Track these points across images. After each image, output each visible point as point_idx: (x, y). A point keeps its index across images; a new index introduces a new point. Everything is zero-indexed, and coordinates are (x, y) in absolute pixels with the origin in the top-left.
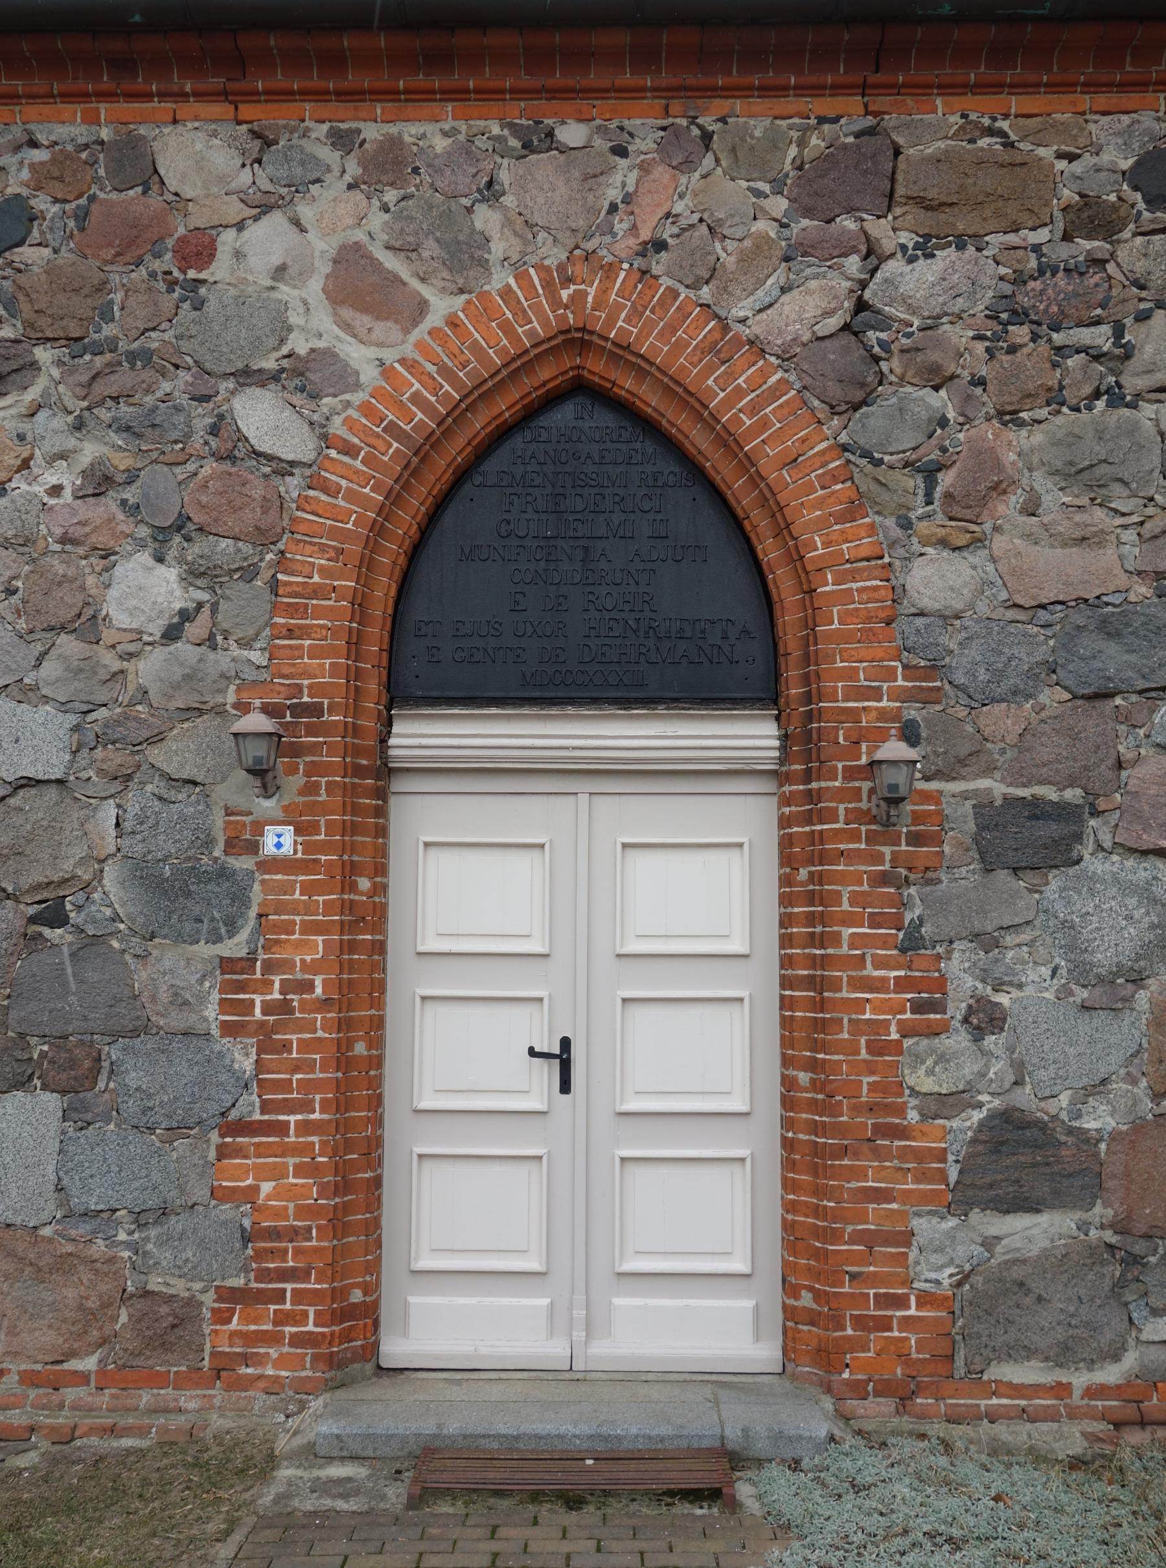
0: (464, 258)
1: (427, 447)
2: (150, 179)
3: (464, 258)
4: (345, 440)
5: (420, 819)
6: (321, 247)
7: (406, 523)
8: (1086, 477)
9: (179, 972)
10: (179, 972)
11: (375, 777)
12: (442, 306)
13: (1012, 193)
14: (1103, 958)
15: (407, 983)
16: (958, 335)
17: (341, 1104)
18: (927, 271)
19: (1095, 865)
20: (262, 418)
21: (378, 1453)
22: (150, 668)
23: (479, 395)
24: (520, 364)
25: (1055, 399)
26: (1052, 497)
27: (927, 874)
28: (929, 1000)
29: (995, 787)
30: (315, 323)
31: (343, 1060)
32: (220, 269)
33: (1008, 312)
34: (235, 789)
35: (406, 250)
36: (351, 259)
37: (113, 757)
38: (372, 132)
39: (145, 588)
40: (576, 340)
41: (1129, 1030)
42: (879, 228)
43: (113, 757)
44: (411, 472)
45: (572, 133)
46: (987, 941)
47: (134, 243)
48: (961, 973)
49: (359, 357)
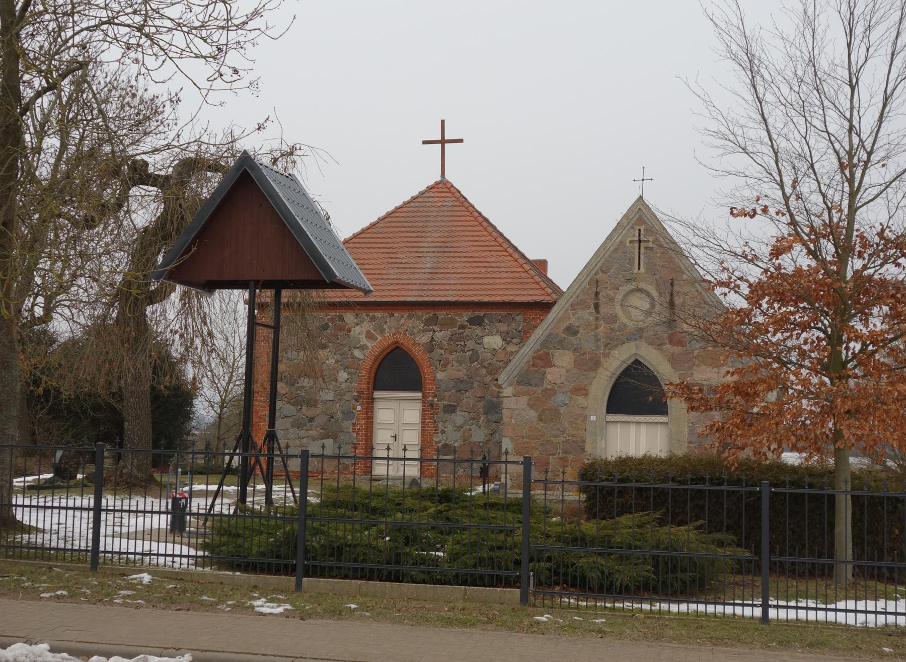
0: (382, 331)
1: (377, 357)
2: (343, 320)
3: (382, 331)
5: (378, 405)
6: (364, 330)
7: (376, 366)
8: (460, 362)
9: (347, 424)
10: (347, 424)
11: (371, 400)
12: (380, 338)
13: (452, 323)
14: (458, 424)
15: (376, 427)
16: (444, 343)
17: (366, 441)
18: (441, 334)
19: (458, 413)
20: (357, 353)
21: (332, 314)
22: (343, 386)
23: (384, 350)
24: (389, 346)
25: (456, 351)
26: (455, 364)
27: (437, 413)
28: (436, 429)
29: (446, 402)
30: (364, 341)
31: (366, 436)
32: (352, 333)
33: (451, 339)
34: (353, 402)
35: (375, 330)
36: (368, 332)
37: (339, 397)
38: (371, 314)
39: (343, 375)
41: (460, 434)
42: (435, 328)
43: (339, 397)
44: (375, 361)
45: (396, 315)
46: (444, 422)
47: (341, 329)
48: (440, 426)
49: (369, 345)
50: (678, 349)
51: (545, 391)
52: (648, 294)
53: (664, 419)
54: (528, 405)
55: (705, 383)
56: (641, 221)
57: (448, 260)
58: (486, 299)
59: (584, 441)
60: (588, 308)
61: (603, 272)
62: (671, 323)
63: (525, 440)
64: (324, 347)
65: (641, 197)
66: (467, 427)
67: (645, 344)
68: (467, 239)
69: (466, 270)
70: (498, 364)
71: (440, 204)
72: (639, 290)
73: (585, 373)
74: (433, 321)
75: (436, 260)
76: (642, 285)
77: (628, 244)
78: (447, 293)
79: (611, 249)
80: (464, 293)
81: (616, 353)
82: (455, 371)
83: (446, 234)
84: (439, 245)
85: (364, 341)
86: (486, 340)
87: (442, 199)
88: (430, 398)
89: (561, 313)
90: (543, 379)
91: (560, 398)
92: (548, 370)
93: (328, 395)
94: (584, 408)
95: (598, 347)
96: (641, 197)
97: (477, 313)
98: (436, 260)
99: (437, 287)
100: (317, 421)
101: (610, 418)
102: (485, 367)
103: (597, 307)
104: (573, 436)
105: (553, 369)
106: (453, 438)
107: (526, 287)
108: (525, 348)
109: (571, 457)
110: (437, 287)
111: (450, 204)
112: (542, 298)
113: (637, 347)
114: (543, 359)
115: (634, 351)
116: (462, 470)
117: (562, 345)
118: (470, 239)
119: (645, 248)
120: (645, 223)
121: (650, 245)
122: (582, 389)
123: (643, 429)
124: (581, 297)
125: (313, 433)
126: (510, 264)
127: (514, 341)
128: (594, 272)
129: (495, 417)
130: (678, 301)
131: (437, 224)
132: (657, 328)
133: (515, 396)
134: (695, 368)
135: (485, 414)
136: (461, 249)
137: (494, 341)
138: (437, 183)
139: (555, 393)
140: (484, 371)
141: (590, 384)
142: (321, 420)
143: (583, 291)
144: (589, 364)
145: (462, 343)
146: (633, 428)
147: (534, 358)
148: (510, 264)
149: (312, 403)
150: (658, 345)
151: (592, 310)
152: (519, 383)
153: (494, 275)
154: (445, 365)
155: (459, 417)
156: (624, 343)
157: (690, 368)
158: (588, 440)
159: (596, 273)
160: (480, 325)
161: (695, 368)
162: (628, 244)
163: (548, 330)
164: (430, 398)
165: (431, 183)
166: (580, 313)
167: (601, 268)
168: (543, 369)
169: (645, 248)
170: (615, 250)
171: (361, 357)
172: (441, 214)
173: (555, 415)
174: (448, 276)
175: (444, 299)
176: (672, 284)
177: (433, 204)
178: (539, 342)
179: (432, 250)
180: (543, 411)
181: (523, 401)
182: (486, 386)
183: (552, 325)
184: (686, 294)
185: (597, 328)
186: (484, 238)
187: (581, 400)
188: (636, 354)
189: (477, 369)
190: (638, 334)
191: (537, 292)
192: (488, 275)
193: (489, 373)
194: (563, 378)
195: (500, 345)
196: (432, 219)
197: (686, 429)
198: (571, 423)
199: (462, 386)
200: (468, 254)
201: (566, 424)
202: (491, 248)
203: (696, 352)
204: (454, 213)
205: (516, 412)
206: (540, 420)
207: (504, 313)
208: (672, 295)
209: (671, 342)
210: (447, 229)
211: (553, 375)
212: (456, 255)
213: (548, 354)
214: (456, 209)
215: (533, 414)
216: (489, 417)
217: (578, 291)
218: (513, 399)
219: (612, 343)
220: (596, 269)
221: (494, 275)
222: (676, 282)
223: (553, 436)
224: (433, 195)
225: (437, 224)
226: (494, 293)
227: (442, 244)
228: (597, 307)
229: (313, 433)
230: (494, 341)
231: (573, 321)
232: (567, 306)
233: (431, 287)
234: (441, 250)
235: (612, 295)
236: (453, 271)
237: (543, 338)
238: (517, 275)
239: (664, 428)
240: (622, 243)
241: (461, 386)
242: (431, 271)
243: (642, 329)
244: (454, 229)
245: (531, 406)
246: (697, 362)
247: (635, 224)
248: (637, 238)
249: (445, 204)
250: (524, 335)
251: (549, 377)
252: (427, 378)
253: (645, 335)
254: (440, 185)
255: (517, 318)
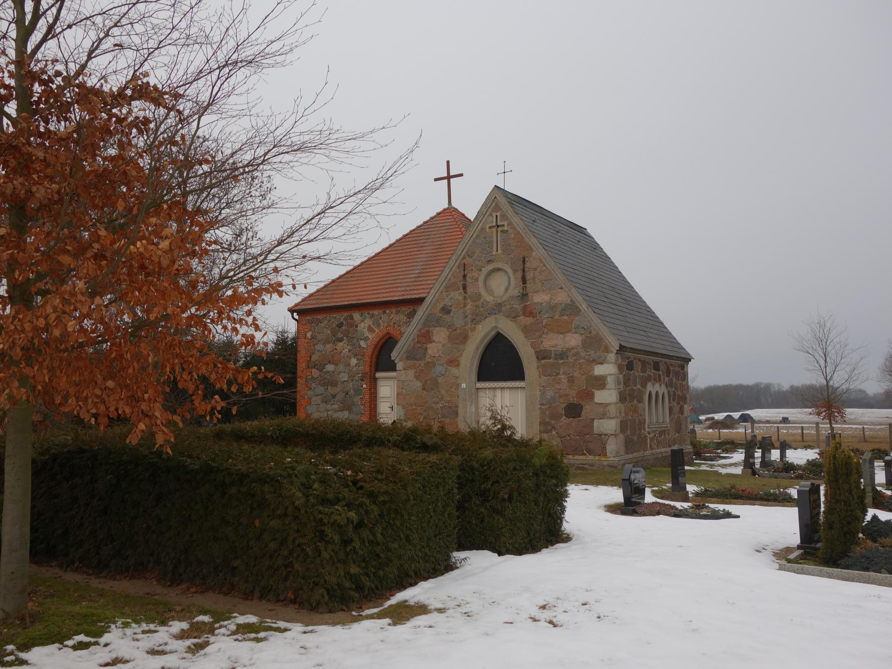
0: (378, 325)
1: (376, 346)
2: (352, 319)
3: (378, 325)
4: (316, 625)
5: (380, 383)
6: (367, 325)
7: (376, 353)
9: (357, 399)
11: (376, 379)
15: (379, 400)
20: (362, 343)
21: (345, 314)
23: (380, 340)
24: (384, 336)
30: (367, 334)
31: (370, 407)
36: (369, 326)
39: (354, 361)
40: (388, 333)
47: (351, 325)
49: (370, 336)
50: (529, 320)
51: (428, 363)
53: (394, 374)
59: (457, 407)
62: (524, 296)
64: (341, 340)
67: (503, 317)
77: (487, 230)
85: (367, 334)
91: (439, 369)
92: (429, 346)
93: (344, 377)
94: (457, 378)
95: (466, 323)
100: (339, 397)
101: (480, 385)
104: (449, 402)
113: (497, 320)
114: (425, 337)
117: (438, 323)
119: (502, 231)
121: (505, 228)
123: (507, 393)
124: (453, 280)
125: (335, 407)
139: (434, 365)
141: (461, 356)
142: (340, 396)
146: (498, 393)
147: (418, 336)
149: (334, 384)
150: (514, 317)
151: (461, 291)
152: (408, 358)
156: (486, 317)
157: (540, 336)
158: (460, 405)
159: (464, 258)
162: (487, 230)
165: (440, 209)
167: (467, 252)
169: (502, 231)
171: (365, 346)
180: (426, 382)
185: (465, 306)
187: (454, 370)
190: (498, 308)
198: (447, 391)
203: (545, 321)
208: (524, 271)
209: (524, 314)
211: (433, 349)
213: (428, 332)
215: (419, 384)
219: (477, 318)
222: (527, 259)
229: (335, 407)
231: (447, 302)
240: (483, 229)
243: (500, 304)
247: (493, 211)
250: (411, 315)
251: (430, 352)
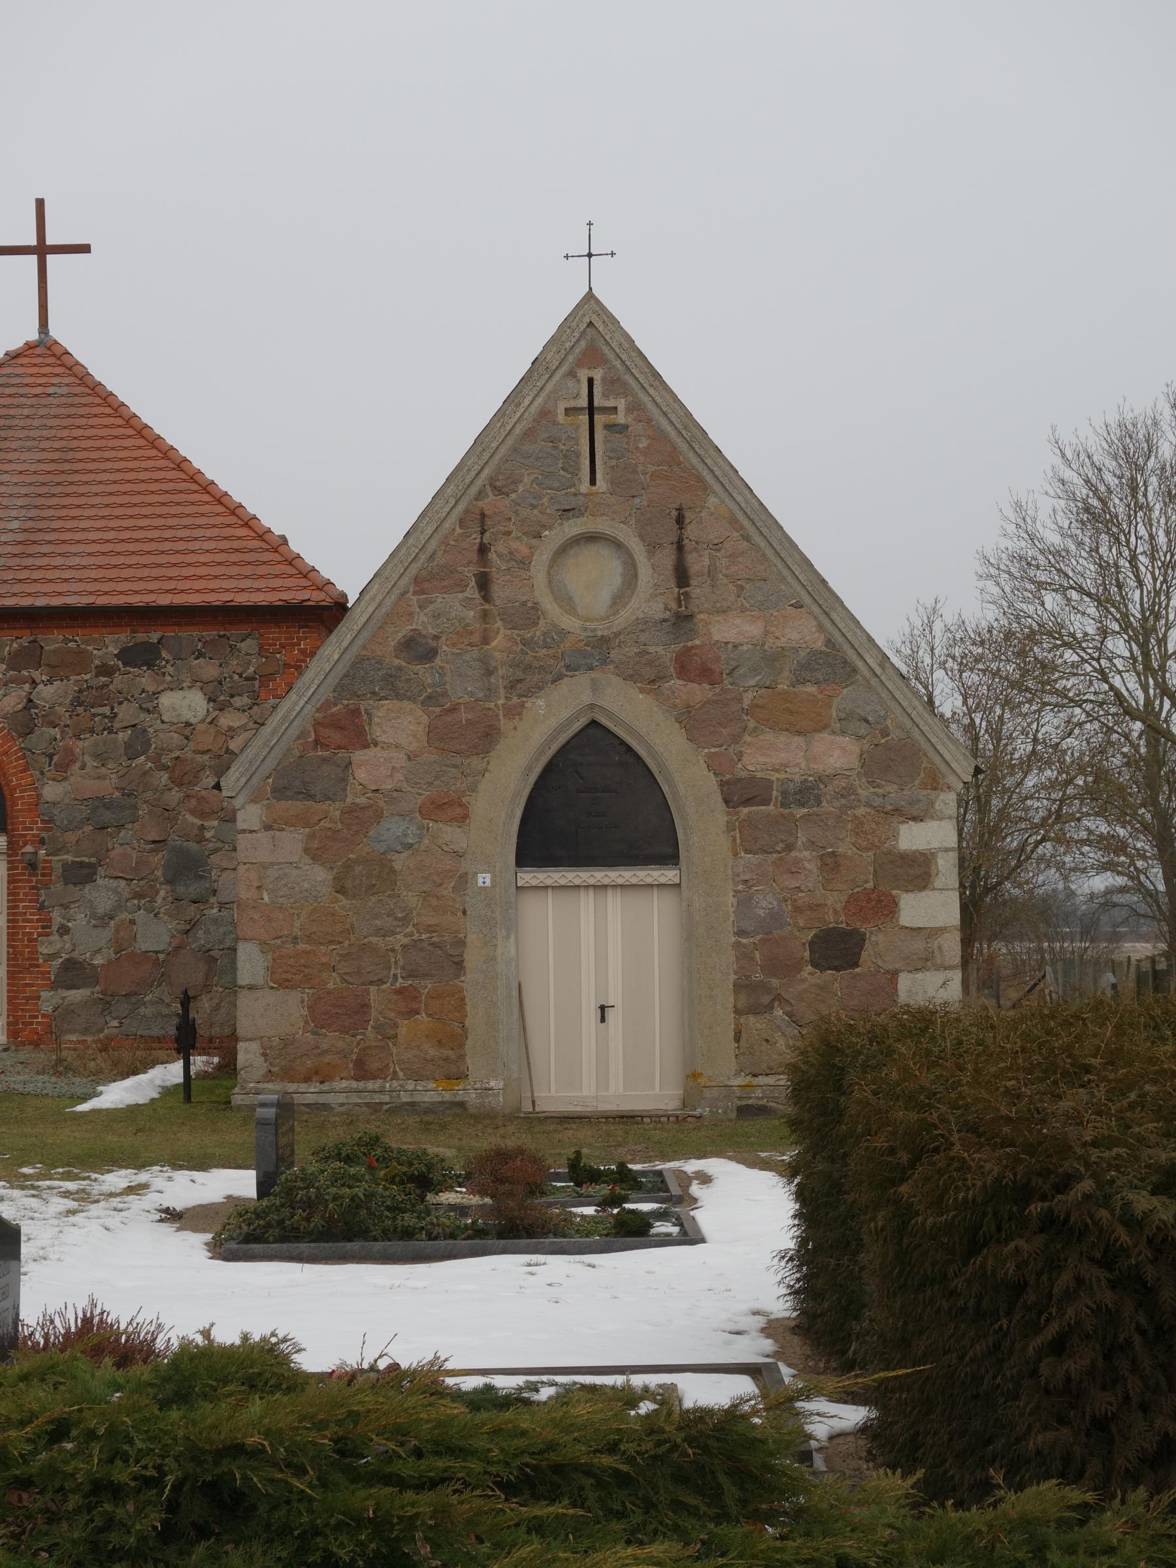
8: (102, 758)
13: (77, 661)
14: (100, 911)
16: (60, 710)
18: (50, 689)
19: (100, 882)
25: (92, 731)
26: (90, 762)
27: (46, 886)
28: (46, 923)
29: (69, 858)
33: (77, 702)
41: (107, 934)
42: (36, 675)
46: (66, 907)
48: (57, 916)
50: (699, 692)
52: (618, 545)
53: (669, 875)
54: (306, 850)
55: (775, 776)
56: (592, 355)
57: (64, 512)
58: (164, 600)
59: (462, 943)
60: (462, 586)
61: (498, 491)
63: (302, 946)
65: (590, 296)
66: (124, 916)
67: (616, 680)
68: (109, 465)
69: (111, 535)
70: (199, 758)
71: (39, 390)
72: (592, 538)
73: (458, 760)
74: (30, 657)
75: (33, 513)
76: (602, 525)
77: (561, 417)
78: (64, 587)
79: (518, 431)
80: (106, 587)
81: (539, 704)
82: (91, 779)
83: (57, 455)
84: (41, 479)
86: (167, 700)
87: (43, 380)
88: (29, 849)
89: (389, 603)
90: (344, 780)
91: (392, 829)
92: (358, 756)
94: (458, 855)
95: (491, 692)
96: (590, 296)
97: (141, 637)
98: (33, 513)
99: (37, 575)
101: (529, 877)
102: (165, 768)
103: (484, 583)
104: (430, 929)
105: (372, 752)
106: (91, 944)
107: (262, 570)
108: (293, 696)
109: (427, 986)
110: (37, 575)
111: (65, 390)
112: (305, 595)
113: (595, 687)
114: (343, 728)
115: (586, 698)
116: (115, 1023)
117: (392, 686)
118: (116, 466)
120: (603, 361)
121: (621, 418)
122: (450, 804)
123: (614, 902)
126: (218, 520)
127: (238, 702)
128: (473, 491)
129: (194, 889)
130: (697, 563)
131: (33, 434)
132: (643, 637)
133: (268, 828)
134: (747, 738)
135: (170, 882)
136: (95, 489)
137: (186, 704)
138: (29, 346)
139: (379, 816)
140: (164, 778)
141: (473, 788)
143: (444, 542)
144: (468, 737)
145: (106, 710)
146: (587, 901)
147: (317, 724)
148: (218, 520)
150: (649, 679)
151: (472, 592)
152: (280, 792)
153: (181, 546)
154: (64, 765)
155: (103, 893)
156: (560, 677)
157: (736, 739)
158: (472, 939)
159: (480, 495)
160: (150, 665)
161: (747, 738)
162: (561, 417)
163: (355, 649)
164: (29, 849)
165: (16, 344)
166: (441, 601)
167: (492, 480)
168: (342, 754)
169: (609, 427)
170: (529, 434)
172: (42, 412)
173: (382, 874)
174: (65, 548)
175: (56, 602)
176: (680, 521)
177: (22, 391)
178: (332, 681)
179: (24, 491)
180: (348, 866)
181: (292, 842)
182: (168, 814)
183: (366, 634)
184: (717, 546)
185: (486, 640)
186: (151, 464)
187: (450, 834)
188: (592, 706)
189: (145, 773)
190: (596, 652)
191: (289, 582)
192: (167, 546)
193: (178, 782)
194: (399, 776)
195: (202, 713)
196: (21, 423)
197: (731, 900)
198: (426, 895)
199: (108, 816)
200: (112, 499)
201: (411, 899)
202: (170, 486)
204: (73, 411)
205: (273, 873)
206: (341, 890)
207: (211, 634)
208: (680, 547)
210: (57, 445)
211: (371, 769)
212: (82, 500)
213: (356, 712)
214: (77, 400)
215: (320, 876)
216: (181, 889)
217: (433, 545)
218: (264, 836)
219: (528, 678)
220: (479, 483)
221: (181, 546)
222: (689, 515)
223: (379, 932)
224: (21, 370)
225: (33, 434)
226: (181, 585)
227: (48, 478)
228: (484, 583)
230: (186, 704)
231: (422, 621)
232: (402, 583)
233: (24, 574)
234: (44, 490)
235: (525, 551)
236: (77, 536)
237: (341, 669)
238: (236, 544)
239: (669, 897)
241: (105, 815)
242: (21, 537)
243: (604, 640)
244: (75, 444)
245: (314, 854)
246: (752, 724)
247: (580, 364)
248: (584, 403)
249: (51, 390)
250: (266, 686)
251: (361, 774)
252: (20, 800)
253: (613, 655)
254: (38, 351)
255: (243, 646)
